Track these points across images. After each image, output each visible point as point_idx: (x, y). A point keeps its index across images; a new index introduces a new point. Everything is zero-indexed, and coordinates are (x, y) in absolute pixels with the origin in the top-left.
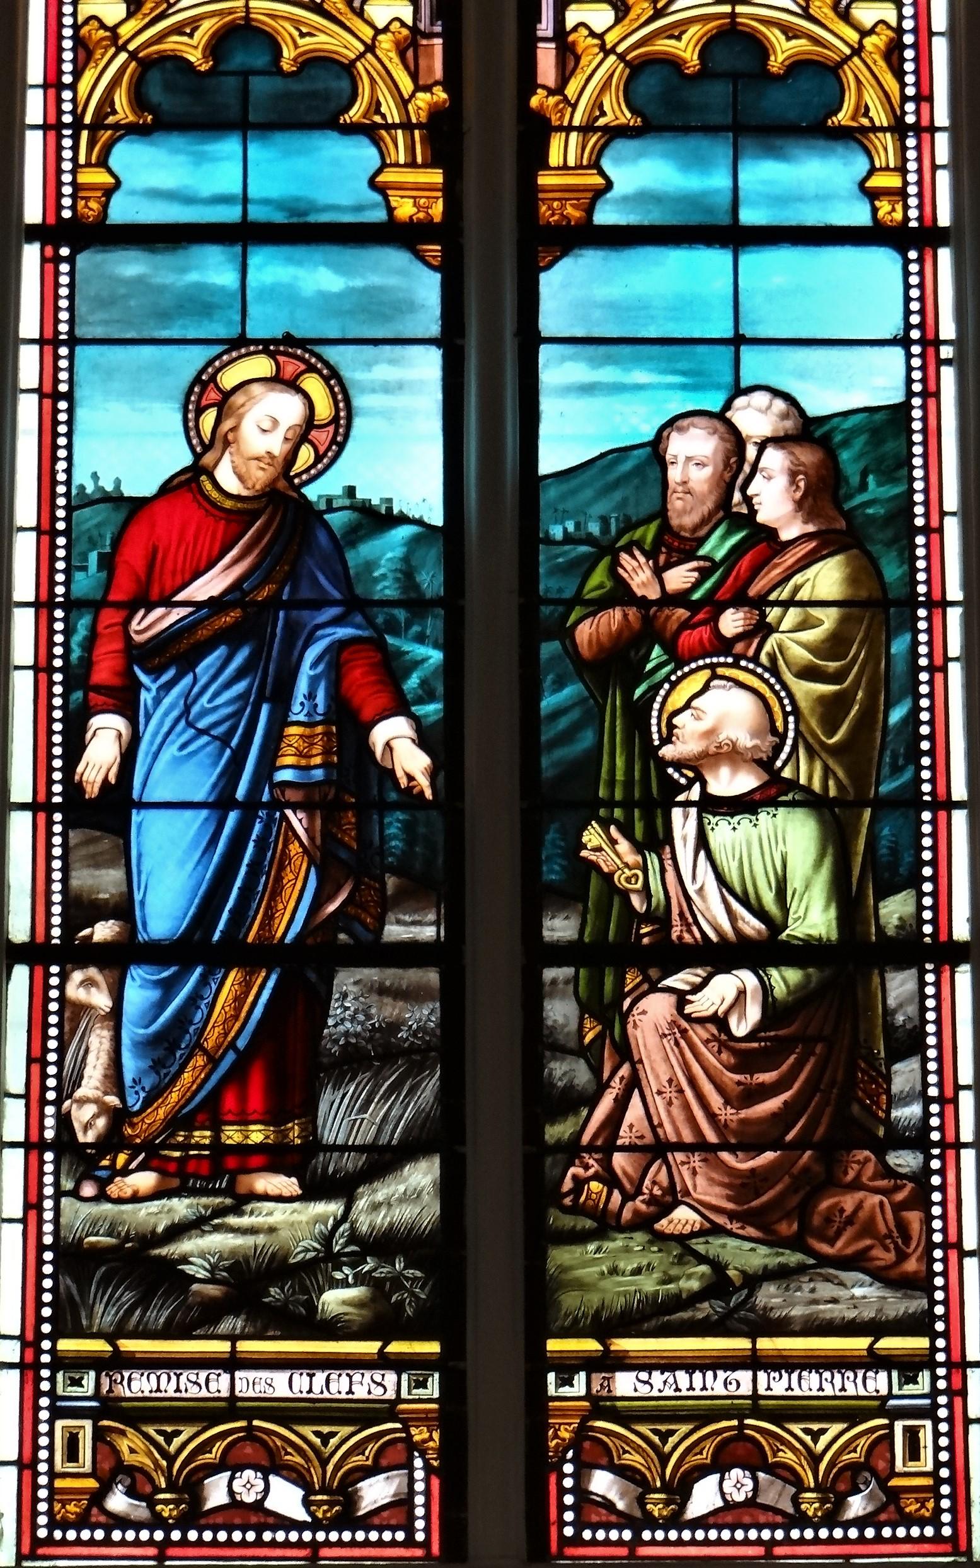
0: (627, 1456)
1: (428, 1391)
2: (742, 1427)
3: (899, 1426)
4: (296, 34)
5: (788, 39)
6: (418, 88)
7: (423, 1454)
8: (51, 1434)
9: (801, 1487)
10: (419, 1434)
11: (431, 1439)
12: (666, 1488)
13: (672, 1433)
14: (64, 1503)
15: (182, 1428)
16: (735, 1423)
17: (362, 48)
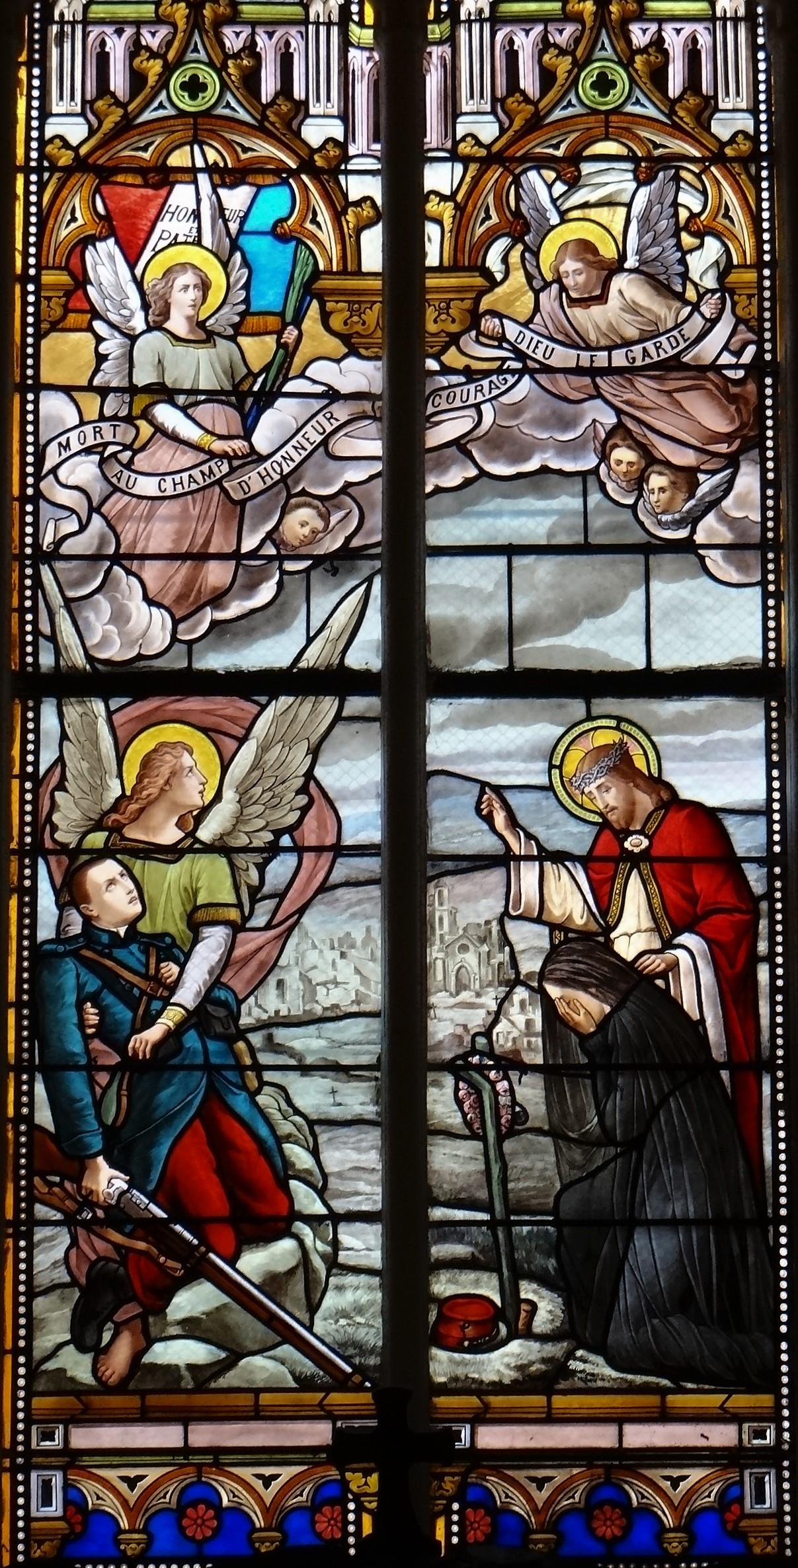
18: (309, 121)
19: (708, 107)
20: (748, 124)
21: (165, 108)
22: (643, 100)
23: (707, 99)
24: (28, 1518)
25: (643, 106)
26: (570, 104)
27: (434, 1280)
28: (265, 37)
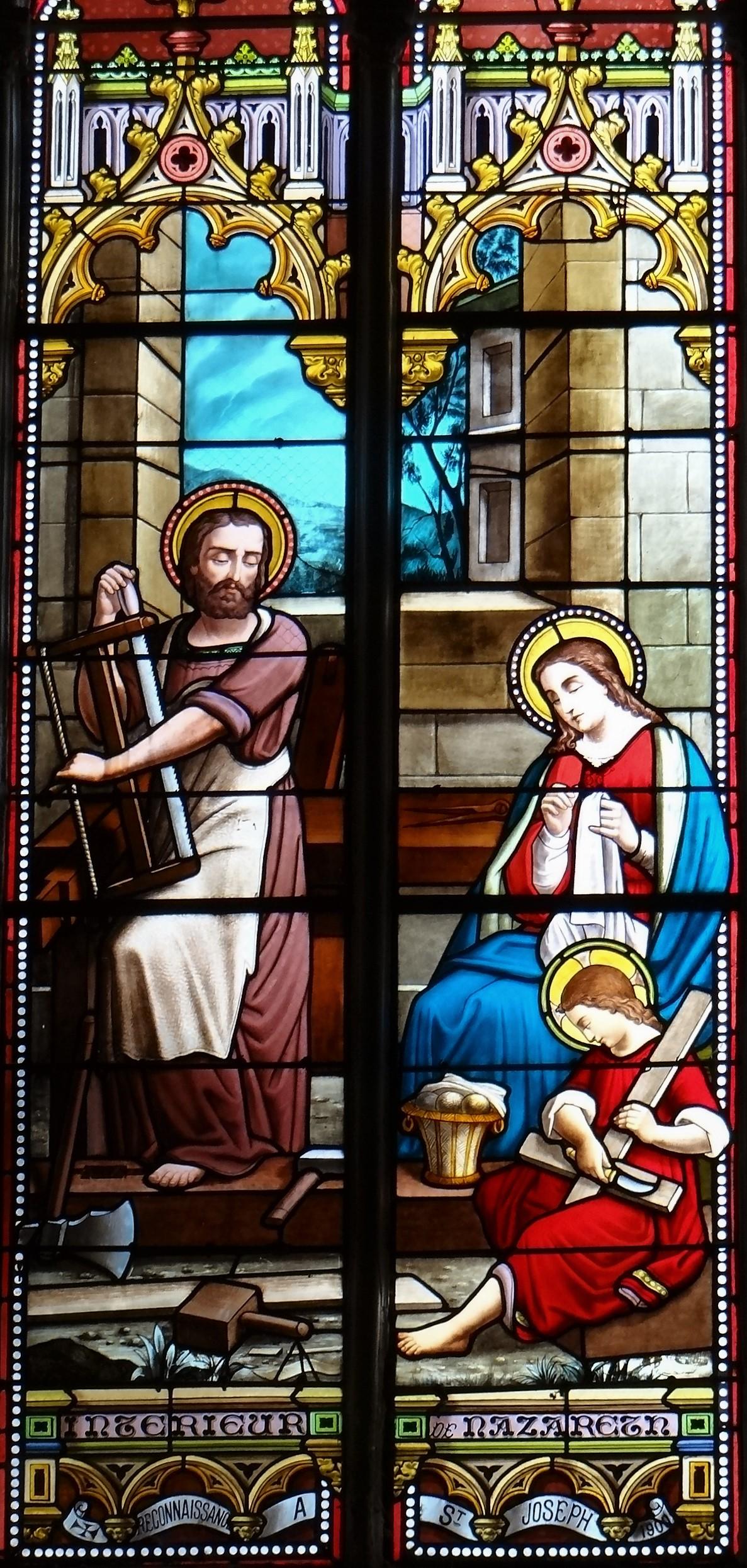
0: (217, 1486)
1: (690, 1418)
2: (184, 1462)
3: (686, 1462)
4: (224, 214)
5: (72, 284)
6: (328, 257)
7: (329, 1481)
8: (21, 1468)
9: (234, 1513)
10: (326, 1466)
11: (336, 1468)
12: (121, 1514)
13: (496, 1468)
14: (33, 1529)
15: (259, 1461)
16: (179, 1458)
17: (280, 224)
18: (290, 185)
19: (282, 176)
20: (702, 184)
21: (157, 179)
22: (221, 173)
23: (279, 169)
24: (717, 1455)
25: (220, 179)
26: (154, 177)
27: (38, 1299)
28: (633, 100)
